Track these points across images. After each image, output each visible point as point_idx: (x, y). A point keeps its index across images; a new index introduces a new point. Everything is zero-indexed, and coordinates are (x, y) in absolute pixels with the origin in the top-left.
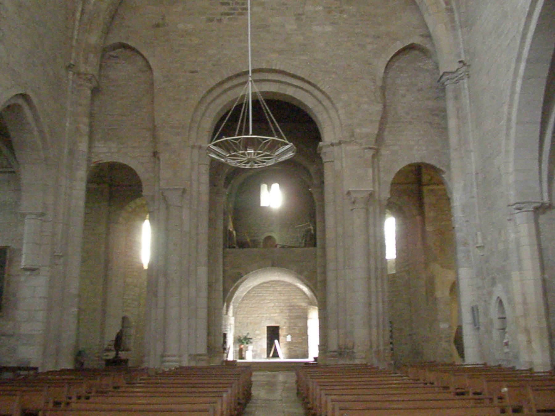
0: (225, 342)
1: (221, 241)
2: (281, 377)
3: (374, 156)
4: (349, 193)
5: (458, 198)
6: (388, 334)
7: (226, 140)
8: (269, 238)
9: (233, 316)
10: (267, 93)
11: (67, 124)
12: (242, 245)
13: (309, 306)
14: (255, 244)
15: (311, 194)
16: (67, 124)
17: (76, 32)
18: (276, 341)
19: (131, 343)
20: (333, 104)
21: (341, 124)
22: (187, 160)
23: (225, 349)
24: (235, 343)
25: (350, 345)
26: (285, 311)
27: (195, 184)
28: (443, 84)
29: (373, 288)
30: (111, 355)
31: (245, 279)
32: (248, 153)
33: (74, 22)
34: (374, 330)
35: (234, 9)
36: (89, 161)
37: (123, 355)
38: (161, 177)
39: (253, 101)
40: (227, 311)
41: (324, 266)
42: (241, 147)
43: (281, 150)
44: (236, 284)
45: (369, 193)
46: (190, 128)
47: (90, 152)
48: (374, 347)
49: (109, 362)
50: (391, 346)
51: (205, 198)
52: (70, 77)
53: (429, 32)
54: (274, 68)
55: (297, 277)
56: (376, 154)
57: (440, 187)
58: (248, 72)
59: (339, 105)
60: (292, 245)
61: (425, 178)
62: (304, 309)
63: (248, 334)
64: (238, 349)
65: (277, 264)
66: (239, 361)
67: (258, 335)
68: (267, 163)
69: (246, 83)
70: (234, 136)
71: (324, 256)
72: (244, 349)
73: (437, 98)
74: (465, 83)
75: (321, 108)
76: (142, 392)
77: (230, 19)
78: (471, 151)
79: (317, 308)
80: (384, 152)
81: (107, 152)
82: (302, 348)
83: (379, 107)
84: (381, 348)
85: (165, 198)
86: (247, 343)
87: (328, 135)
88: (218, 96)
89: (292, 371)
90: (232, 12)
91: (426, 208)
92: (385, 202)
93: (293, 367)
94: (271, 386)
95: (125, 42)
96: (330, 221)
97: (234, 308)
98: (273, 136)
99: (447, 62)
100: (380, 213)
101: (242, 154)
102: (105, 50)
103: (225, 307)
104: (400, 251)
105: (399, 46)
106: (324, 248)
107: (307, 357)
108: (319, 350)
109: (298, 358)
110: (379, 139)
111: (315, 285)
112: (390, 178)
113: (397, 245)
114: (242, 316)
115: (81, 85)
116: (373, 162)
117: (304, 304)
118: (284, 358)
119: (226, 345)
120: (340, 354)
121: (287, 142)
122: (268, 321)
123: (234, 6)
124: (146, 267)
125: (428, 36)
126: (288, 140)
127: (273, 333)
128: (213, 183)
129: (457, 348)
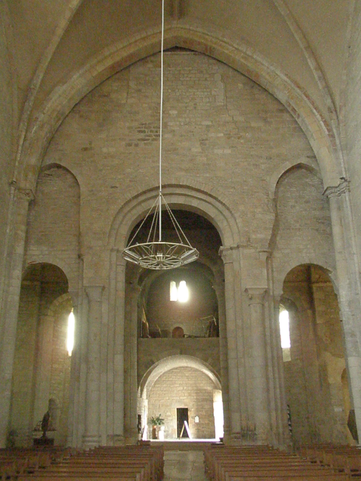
0: (140, 423)
1: (136, 333)
2: (191, 456)
3: (268, 258)
4: (246, 290)
5: (344, 295)
6: (287, 417)
7: (139, 246)
8: (178, 329)
9: (147, 398)
10: (175, 204)
11: (8, 231)
12: (154, 335)
13: (214, 390)
14: (165, 334)
15: (213, 291)
16: (8, 231)
17: (19, 155)
18: (185, 422)
19: (56, 423)
20: (232, 215)
21: (239, 232)
22: (106, 261)
23: (139, 429)
24: (148, 423)
25: (252, 427)
26: (193, 394)
27: (113, 282)
28: (327, 197)
29: (271, 375)
30: (39, 435)
31: (157, 366)
32: (158, 257)
33: (18, 147)
34: (274, 414)
36: (24, 262)
37: (49, 435)
38: (84, 276)
39: (162, 211)
40: (141, 394)
41: (226, 354)
42: (152, 252)
43: (187, 254)
44: (149, 370)
45: (265, 290)
46: (110, 236)
47: (25, 254)
48: (274, 428)
49: (37, 442)
50: (290, 428)
51: (122, 294)
52: (12, 192)
53: (314, 154)
54: (181, 184)
55: (203, 364)
56: (270, 256)
57: (328, 284)
58: (159, 186)
59: (236, 215)
60: (198, 335)
61: (314, 276)
62: (210, 393)
63: (160, 415)
64: (151, 429)
65: (185, 352)
66: (152, 440)
67: (170, 416)
68: (174, 266)
69: (156, 196)
70: (146, 242)
71: (226, 345)
72: (157, 429)
73: (322, 208)
74: (346, 196)
75: (221, 217)
76: (294, 466)
77: (145, 144)
78: (354, 254)
79: (221, 391)
80: (277, 254)
81: (40, 255)
82: (208, 428)
83: (272, 216)
84: (281, 430)
85: (87, 295)
86: (160, 424)
87: (228, 240)
88: (134, 207)
89: (200, 450)
90: (147, 138)
91: (316, 303)
92: (279, 299)
93: (200, 446)
94: (182, 465)
95: (58, 162)
96: (230, 313)
97: (147, 391)
98: (180, 243)
99: (331, 179)
100: (275, 308)
101: (153, 257)
102: (42, 169)
103: (139, 390)
104: (293, 341)
105: (289, 165)
106: (225, 338)
107: (214, 438)
108: (224, 431)
109: (205, 438)
110: (272, 243)
111: (219, 371)
112: (283, 277)
113: (291, 335)
114: (155, 399)
115: (21, 198)
116: (267, 263)
117: (209, 388)
118: (193, 438)
119: (141, 426)
120: (243, 436)
121: (191, 247)
122: (177, 403)
123: (149, 133)
124: (70, 354)
126: (192, 246)
127: (183, 415)
128: (128, 282)
129: (351, 431)
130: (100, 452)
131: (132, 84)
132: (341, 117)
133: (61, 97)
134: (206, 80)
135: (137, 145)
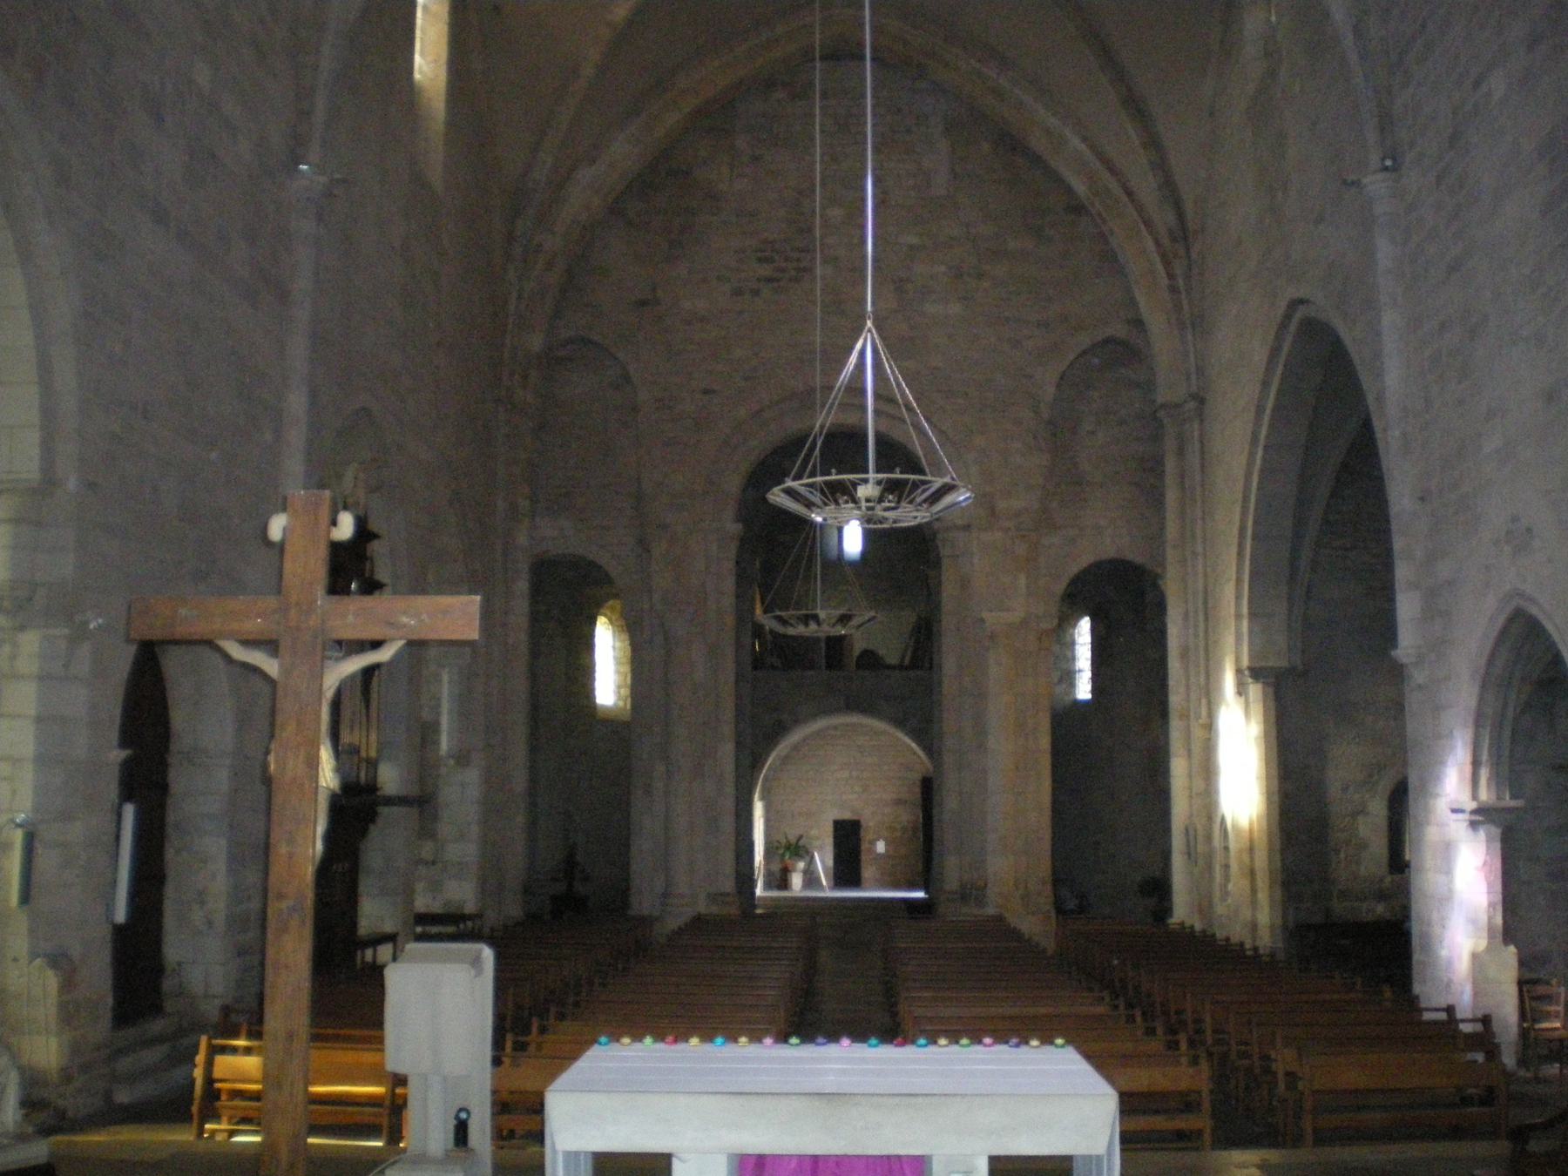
30: (560, 888)
35: (783, 270)
37: (580, 888)
125: (1138, 323)
127: (848, 837)
130: (699, 923)
131: (741, 142)
132: (1194, 256)
133: (585, 194)
134: (909, 131)
135: (756, 293)
